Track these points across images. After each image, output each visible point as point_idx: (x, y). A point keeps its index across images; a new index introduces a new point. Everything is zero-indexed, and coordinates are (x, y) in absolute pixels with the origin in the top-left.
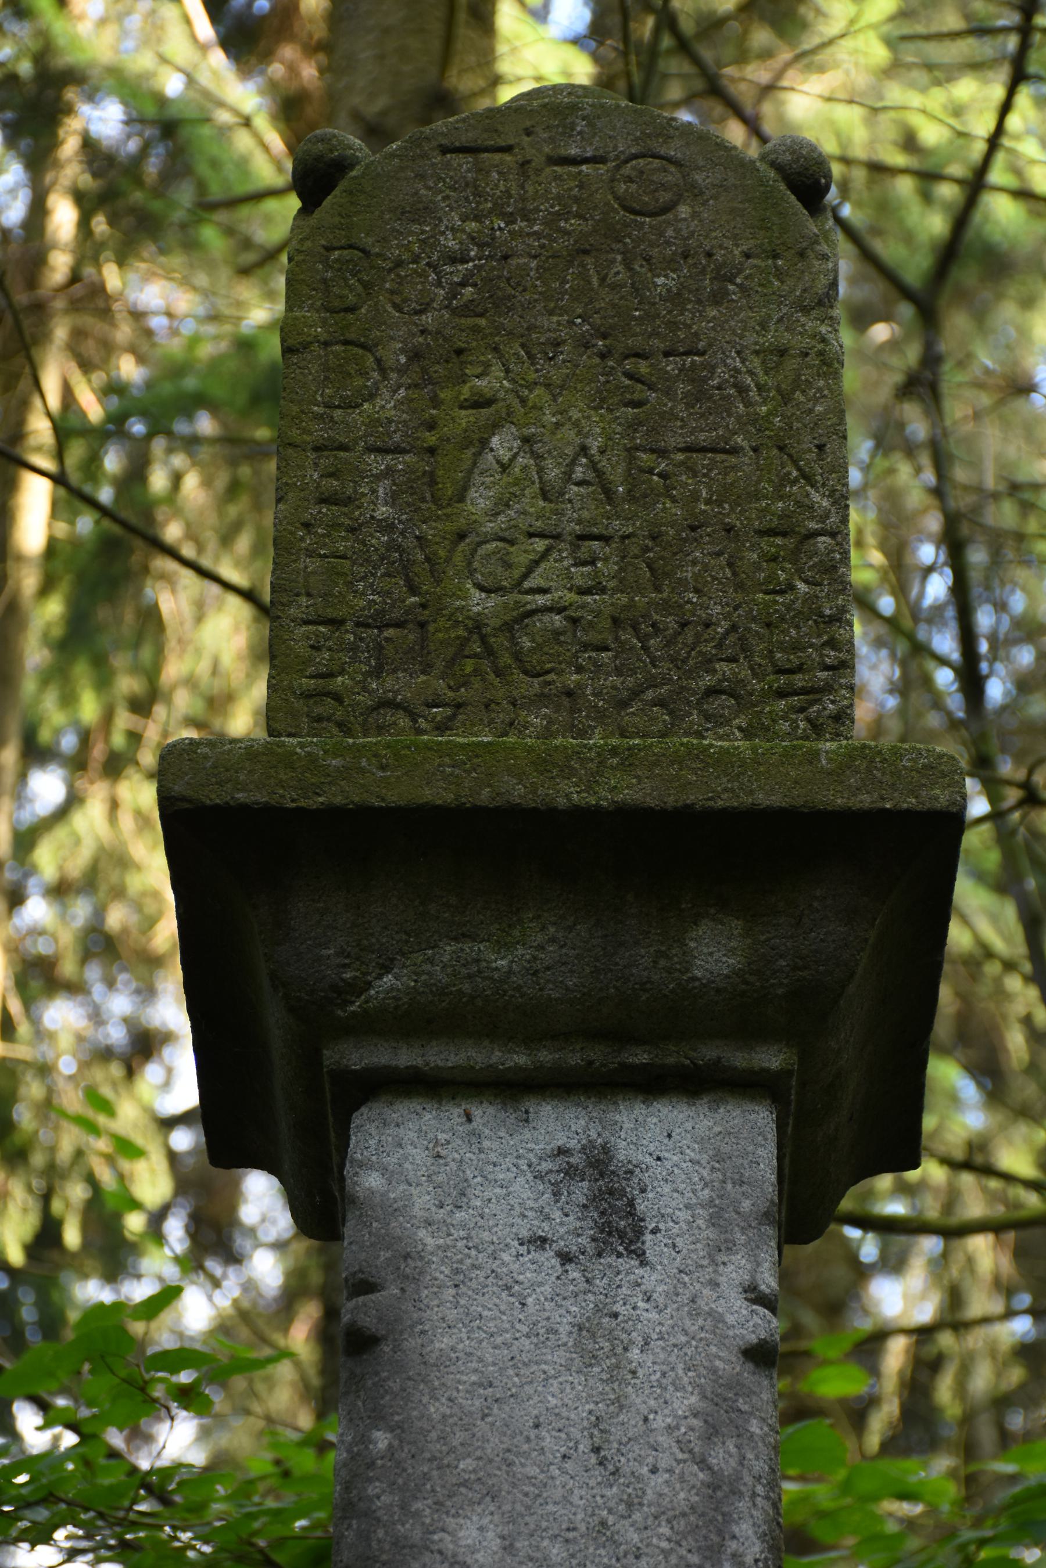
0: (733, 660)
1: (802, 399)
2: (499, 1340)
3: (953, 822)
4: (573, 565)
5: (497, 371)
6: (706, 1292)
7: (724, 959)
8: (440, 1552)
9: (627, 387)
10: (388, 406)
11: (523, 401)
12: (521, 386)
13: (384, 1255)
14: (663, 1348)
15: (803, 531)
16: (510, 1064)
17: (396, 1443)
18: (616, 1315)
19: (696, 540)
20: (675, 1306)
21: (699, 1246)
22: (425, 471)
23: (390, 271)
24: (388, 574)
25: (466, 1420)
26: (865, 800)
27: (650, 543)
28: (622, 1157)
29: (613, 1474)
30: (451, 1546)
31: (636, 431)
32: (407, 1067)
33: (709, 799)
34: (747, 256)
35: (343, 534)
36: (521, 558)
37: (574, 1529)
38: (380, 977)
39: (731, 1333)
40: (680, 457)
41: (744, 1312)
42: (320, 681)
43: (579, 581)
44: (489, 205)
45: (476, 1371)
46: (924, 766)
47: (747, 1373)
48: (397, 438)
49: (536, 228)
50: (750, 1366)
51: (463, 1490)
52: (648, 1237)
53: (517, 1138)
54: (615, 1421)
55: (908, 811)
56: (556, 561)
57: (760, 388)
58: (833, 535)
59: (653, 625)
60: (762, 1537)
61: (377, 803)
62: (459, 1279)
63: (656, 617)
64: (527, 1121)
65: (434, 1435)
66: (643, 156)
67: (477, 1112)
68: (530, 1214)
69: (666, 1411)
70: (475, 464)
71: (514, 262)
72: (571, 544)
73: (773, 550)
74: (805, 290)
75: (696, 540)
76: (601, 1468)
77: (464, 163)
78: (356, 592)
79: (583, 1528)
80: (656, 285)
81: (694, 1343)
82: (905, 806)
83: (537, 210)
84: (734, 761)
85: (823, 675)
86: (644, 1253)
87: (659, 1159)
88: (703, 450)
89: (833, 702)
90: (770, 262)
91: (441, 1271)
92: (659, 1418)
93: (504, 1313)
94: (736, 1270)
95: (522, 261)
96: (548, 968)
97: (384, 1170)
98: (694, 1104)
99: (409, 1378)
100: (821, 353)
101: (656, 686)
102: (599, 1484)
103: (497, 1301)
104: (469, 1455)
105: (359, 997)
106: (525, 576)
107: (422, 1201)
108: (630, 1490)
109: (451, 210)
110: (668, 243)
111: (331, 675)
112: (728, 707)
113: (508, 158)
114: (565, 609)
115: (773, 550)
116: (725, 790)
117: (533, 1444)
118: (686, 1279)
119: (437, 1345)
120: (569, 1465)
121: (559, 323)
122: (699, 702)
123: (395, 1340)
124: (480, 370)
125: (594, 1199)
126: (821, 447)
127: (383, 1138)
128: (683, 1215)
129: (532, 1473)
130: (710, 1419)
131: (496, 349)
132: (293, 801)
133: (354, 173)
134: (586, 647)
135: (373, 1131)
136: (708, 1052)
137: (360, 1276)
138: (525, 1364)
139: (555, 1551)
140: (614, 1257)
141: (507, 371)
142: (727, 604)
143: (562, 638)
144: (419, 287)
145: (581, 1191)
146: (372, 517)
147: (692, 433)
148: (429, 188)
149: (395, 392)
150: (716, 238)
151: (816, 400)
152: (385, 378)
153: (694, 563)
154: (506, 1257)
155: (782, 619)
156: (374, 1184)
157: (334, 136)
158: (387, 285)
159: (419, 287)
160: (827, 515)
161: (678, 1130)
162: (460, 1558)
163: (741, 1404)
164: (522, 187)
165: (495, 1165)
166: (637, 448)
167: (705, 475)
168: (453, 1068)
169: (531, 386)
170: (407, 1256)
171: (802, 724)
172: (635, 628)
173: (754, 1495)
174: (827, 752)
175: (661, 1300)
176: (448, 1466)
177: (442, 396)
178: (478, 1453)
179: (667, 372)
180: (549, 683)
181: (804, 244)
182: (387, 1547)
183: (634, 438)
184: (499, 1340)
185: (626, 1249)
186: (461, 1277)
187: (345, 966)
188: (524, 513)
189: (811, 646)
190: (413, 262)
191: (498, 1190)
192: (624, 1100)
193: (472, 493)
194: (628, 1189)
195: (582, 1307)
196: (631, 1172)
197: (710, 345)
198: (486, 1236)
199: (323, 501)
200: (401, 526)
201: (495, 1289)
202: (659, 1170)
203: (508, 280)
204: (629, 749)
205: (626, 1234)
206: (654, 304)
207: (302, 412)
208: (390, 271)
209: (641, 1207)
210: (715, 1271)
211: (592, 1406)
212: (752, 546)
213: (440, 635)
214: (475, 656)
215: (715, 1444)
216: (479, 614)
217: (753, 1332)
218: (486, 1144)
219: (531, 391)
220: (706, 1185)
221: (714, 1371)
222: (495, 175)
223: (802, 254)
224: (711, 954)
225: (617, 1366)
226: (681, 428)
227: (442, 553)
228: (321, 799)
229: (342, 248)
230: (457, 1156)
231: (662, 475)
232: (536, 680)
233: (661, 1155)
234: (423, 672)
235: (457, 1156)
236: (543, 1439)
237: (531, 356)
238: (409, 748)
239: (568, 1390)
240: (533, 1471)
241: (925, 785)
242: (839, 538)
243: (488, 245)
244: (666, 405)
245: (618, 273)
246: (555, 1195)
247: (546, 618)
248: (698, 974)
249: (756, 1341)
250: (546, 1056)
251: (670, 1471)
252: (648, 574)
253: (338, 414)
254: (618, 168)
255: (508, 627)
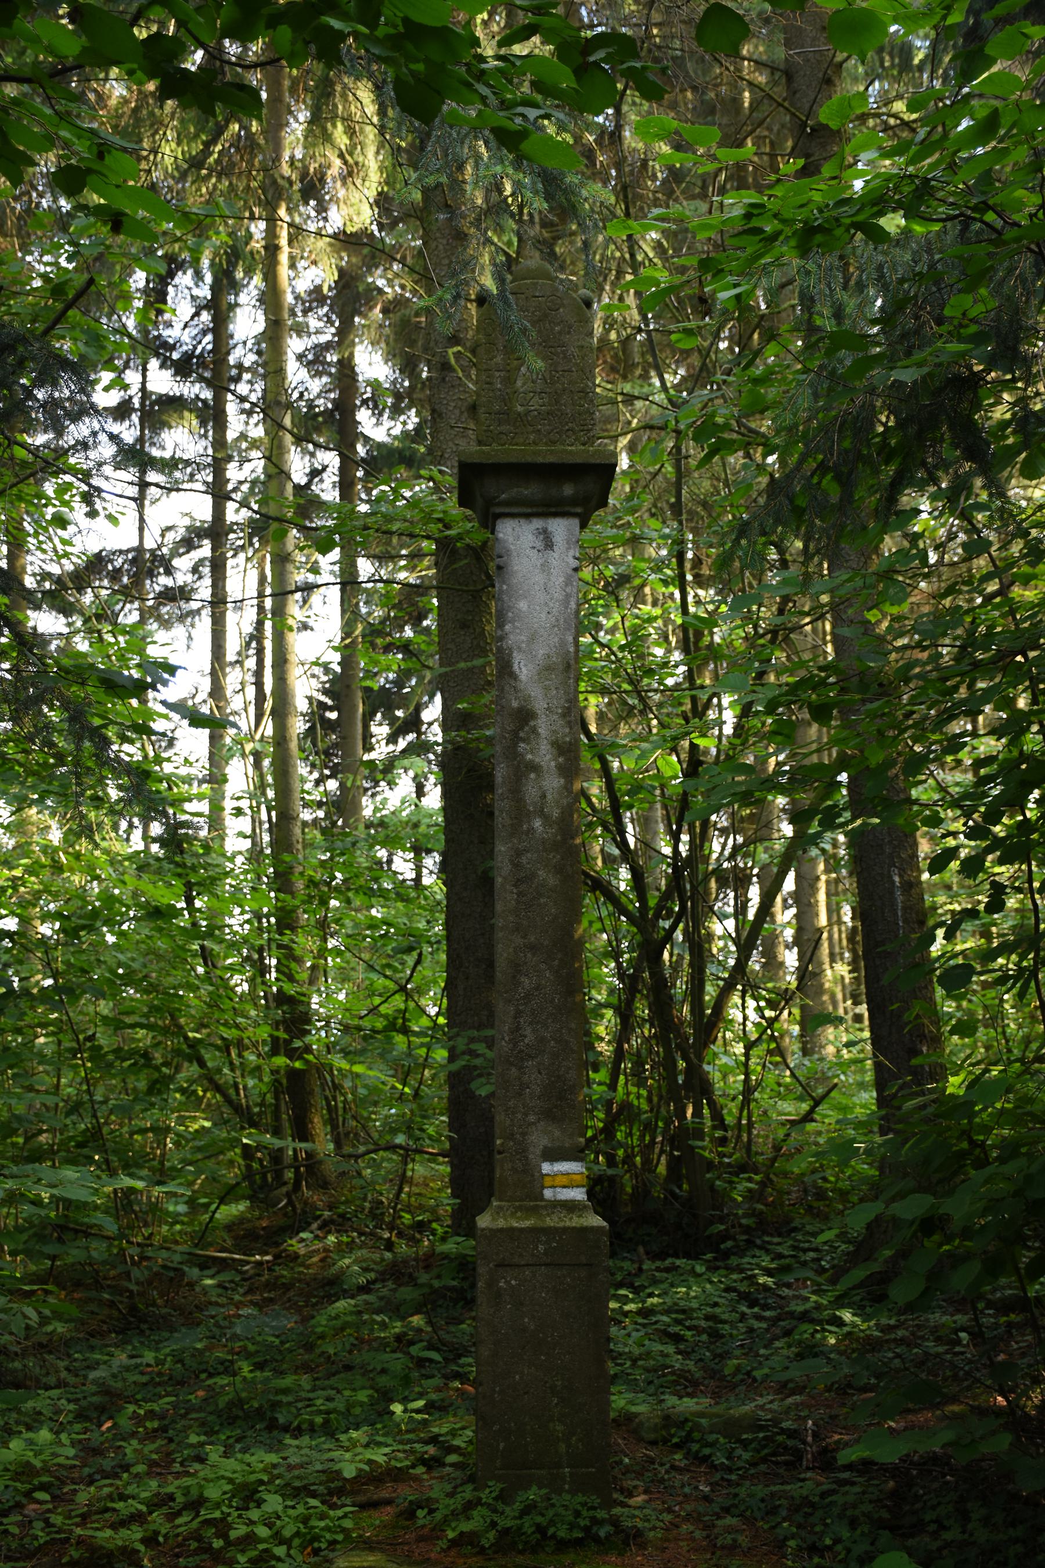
3: (611, 467)
84: (573, 451)
94: (571, 553)
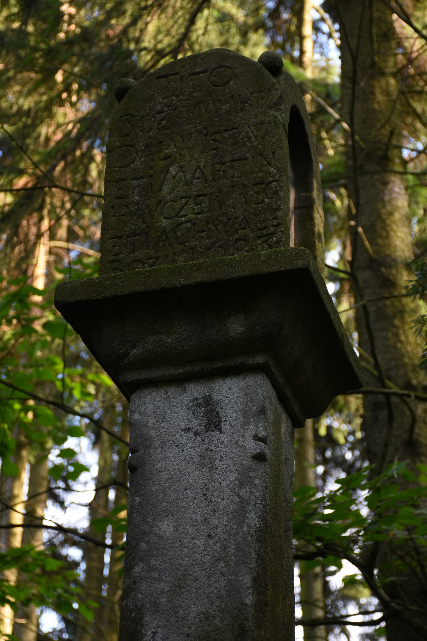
0: (244, 228)
1: (268, 138)
2: (175, 463)
4: (194, 206)
5: (172, 146)
6: (241, 439)
7: (239, 328)
8: (155, 534)
9: (213, 144)
10: (139, 164)
11: (180, 155)
12: (180, 150)
13: (139, 440)
14: (226, 459)
15: (267, 182)
16: (177, 373)
17: (142, 500)
18: (212, 451)
19: (234, 191)
20: (231, 445)
21: (239, 424)
22: (149, 183)
23: (140, 120)
24: (137, 219)
25: (164, 490)
26: (275, 269)
27: (219, 194)
28: (215, 398)
29: (209, 502)
30: (158, 531)
31: (215, 158)
32: (145, 378)
33: (225, 276)
34: (252, 94)
35: (123, 208)
36: (178, 206)
37: (197, 521)
38: (132, 350)
39: (248, 452)
40: (229, 164)
41: (253, 444)
42: (115, 257)
43: (196, 211)
44: (171, 93)
45: (167, 474)
46: (295, 254)
47: (254, 464)
48: (141, 174)
49: (185, 97)
50: (256, 462)
51: (162, 513)
52: (223, 424)
53: (182, 396)
54: (211, 485)
55: (289, 270)
56: (189, 205)
57: (255, 136)
58: (277, 181)
59: (219, 221)
60: (259, 517)
61: (121, 294)
62: (163, 445)
63: (220, 218)
64: (185, 391)
65: (154, 496)
66: (219, 67)
67: (169, 390)
68: (185, 421)
69: (227, 480)
70: (165, 178)
71: (178, 110)
72: (194, 199)
73: (258, 190)
74: (270, 102)
75: (234, 191)
76: (206, 501)
77: (163, 81)
78: (127, 226)
79: (200, 521)
80: (222, 109)
81: (237, 456)
82: (288, 268)
83: (186, 91)
84: (242, 261)
85: (273, 229)
86: (221, 429)
87: (227, 397)
88: (236, 160)
89: (276, 237)
90: (259, 94)
91: (157, 443)
92: (225, 482)
93: (176, 454)
94: (250, 430)
95: (180, 109)
96: (184, 340)
97: (140, 413)
98: (238, 378)
99: (146, 479)
100: (275, 121)
101: (219, 241)
102: (205, 506)
103: (174, 451)
104: (164, 502)
105: (127, 358)
106: (179, 212)
107: (152, 421)
108: (215, 507)
109: (159, 96)
110: (226, 94)
111: (118, 254)
112: (243, 244)
113: (177, 76)
114: (191, 220)
115: (258, 190)
116: (230, 272)
117: (184, 496)
118: (235, 436)
119: (155, 467)
120: (196, 501)
121: (192, 127)
122: (233, 244)
123: (142, 467)
124: (166, 147)
125: (206, 413)
126: (274, 153)
127: (140, 402)
128: (234, 415)
129: (184, 505)
130: (241, 480)
131: (172, 139)
132: (95, 297)
133: (130, 91)
134: (198, 232)
135: (137, 401)
136: (240, 360)
137: (132, 448)
138: (183, 470)
139: (191, 529)
140: (212, 432)
141: (176, 146)
142: (243, 210)
143: (190, 230)
144: (149, 123)
145: (201, 411)
146: (132, 201)
147: (233, 156)
148: (152, 91)
149: (141, 159)
150: (242, 90)
151: (273, 137)
152: (138, 155)
153: (233, 198)
154: (177, 436)
155: (260, 212)
156: (137, 418)
157: (124, 80)
158: (139, 125)
159: (149, 123)
160: (275, 175)
161: (233, 387)
162: (161, 535)
163: (251, 474)
164: (181, 85)
165: (175, 407)
166: (215, 164)
167: (237, 169)
168: (159, 377)
169: (182, 149)
170: (146, 440)
171: (265, 246)
172: (213, 223)
173: (256, 503)
174: (263, 254)
175: (226, 444)
176: (158, 506)
177: (155, 157)
178: (167, 501)
179: (225, 137)
180: (186, 246)
181: (270, 86)
182: (138, 534)
183: (215, 160)
184: (175, 463)
185: (215, 428)
186: (163, 444)
187: (120, 348)
188: (179, 191)
189: (269, 219)
190: (147, 116)
191: (175, 415)
192: (216, 379)
193: (164, 188)
194: (217, 409)
195: (201, 449)
196: (218, 403)
197: (239, 125)
198: (171, 430)
199: (118, 198)
200: (141, 202)
201: (174, 447)
202: (227, 401)
203: (176, 116)
204: (200, 264)
205: (215, 423)
206: (222, 115)
207: (112, 171)
208: (140, 120)
209: (221, 414)
210: (244, 432)
211: (203, 481)
212: (251, 189)
213: (152, 236)
214: (164, 241)
215: (242, 488)
216: (164, 227)
217: (255, 450)
218: (172, 400)
219: (182, 151)
220: (241, 404)
221: (243, 465)
222: (173, 83)
223: (269, 90)
224: (235, 327)
225: (212, 467)
226: (230, 154)
227: (154, 209)
228: (103, 295)
229: (126, 115)
230: (163, 405)
231: (223, 171)
232: (182, 246)
233: (227, 396)
234: (147, 249)
235: (163, 405)
236: (188, 494)
237: (183, 140)
238: (131, 274)
239: (196, 477)
240: (184, 504)
241: (295, 260)
242: (279, 182)
243: (170, 106)
244: (224, 148)
245: (210, 107)
246: (193, 414)
247: (185, 225)
248: (231, 335)
249: (256, 453)
250: (188, 369)
251: (228, 499)
252: (218, 205)
253: (123, 169)
254: (211, 73)
255: (174, 230)
